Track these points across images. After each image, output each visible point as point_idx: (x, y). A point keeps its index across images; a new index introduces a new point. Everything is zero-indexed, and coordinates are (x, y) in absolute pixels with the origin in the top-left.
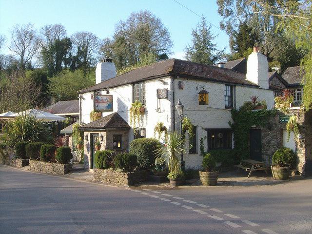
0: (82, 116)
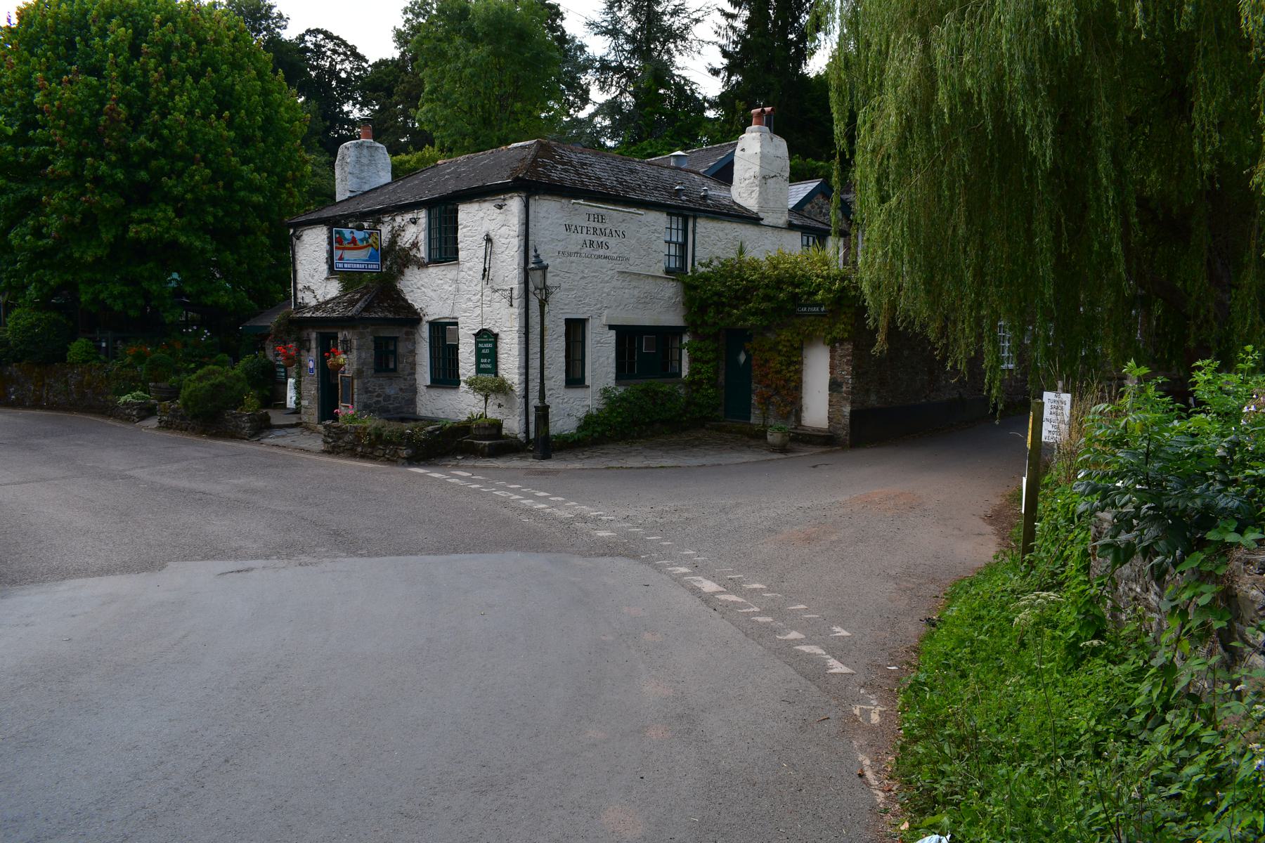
0: (491, 270)
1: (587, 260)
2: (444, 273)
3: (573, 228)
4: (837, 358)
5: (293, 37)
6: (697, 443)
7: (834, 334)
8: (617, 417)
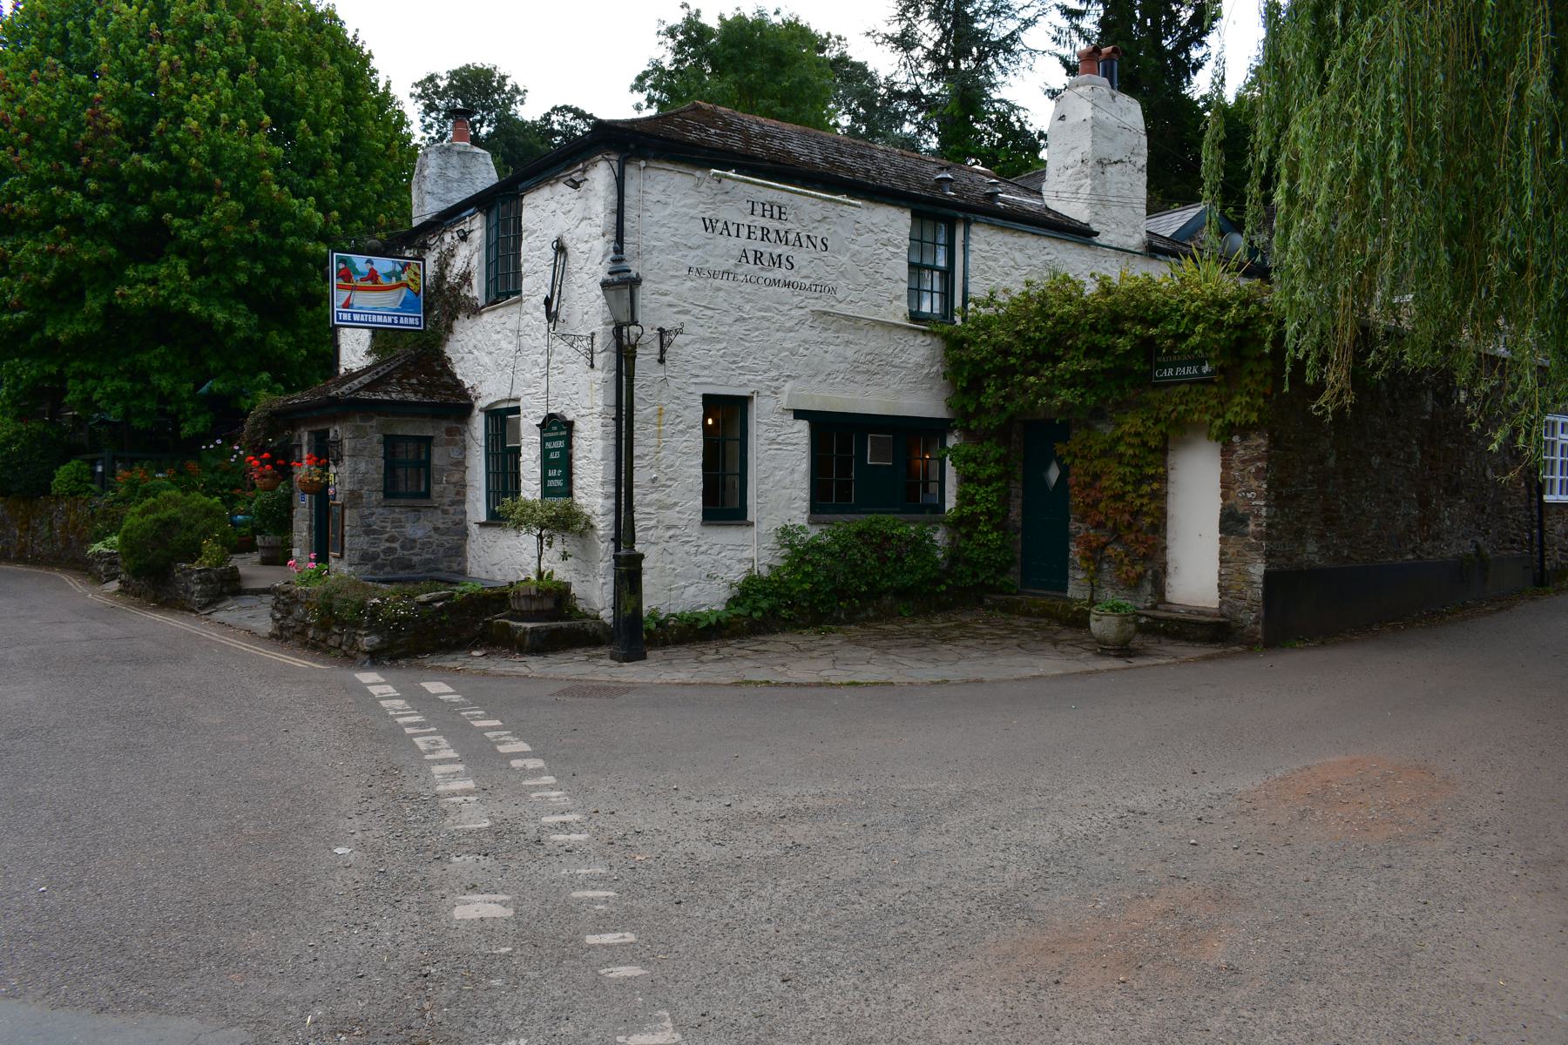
1: (748, 288)
2: (503, 320)
3: (720, 225)
4: (1236, 464)
5: (538, 118)
6: (956, 633)
7: (1229, 416)
8: (801, 582)
